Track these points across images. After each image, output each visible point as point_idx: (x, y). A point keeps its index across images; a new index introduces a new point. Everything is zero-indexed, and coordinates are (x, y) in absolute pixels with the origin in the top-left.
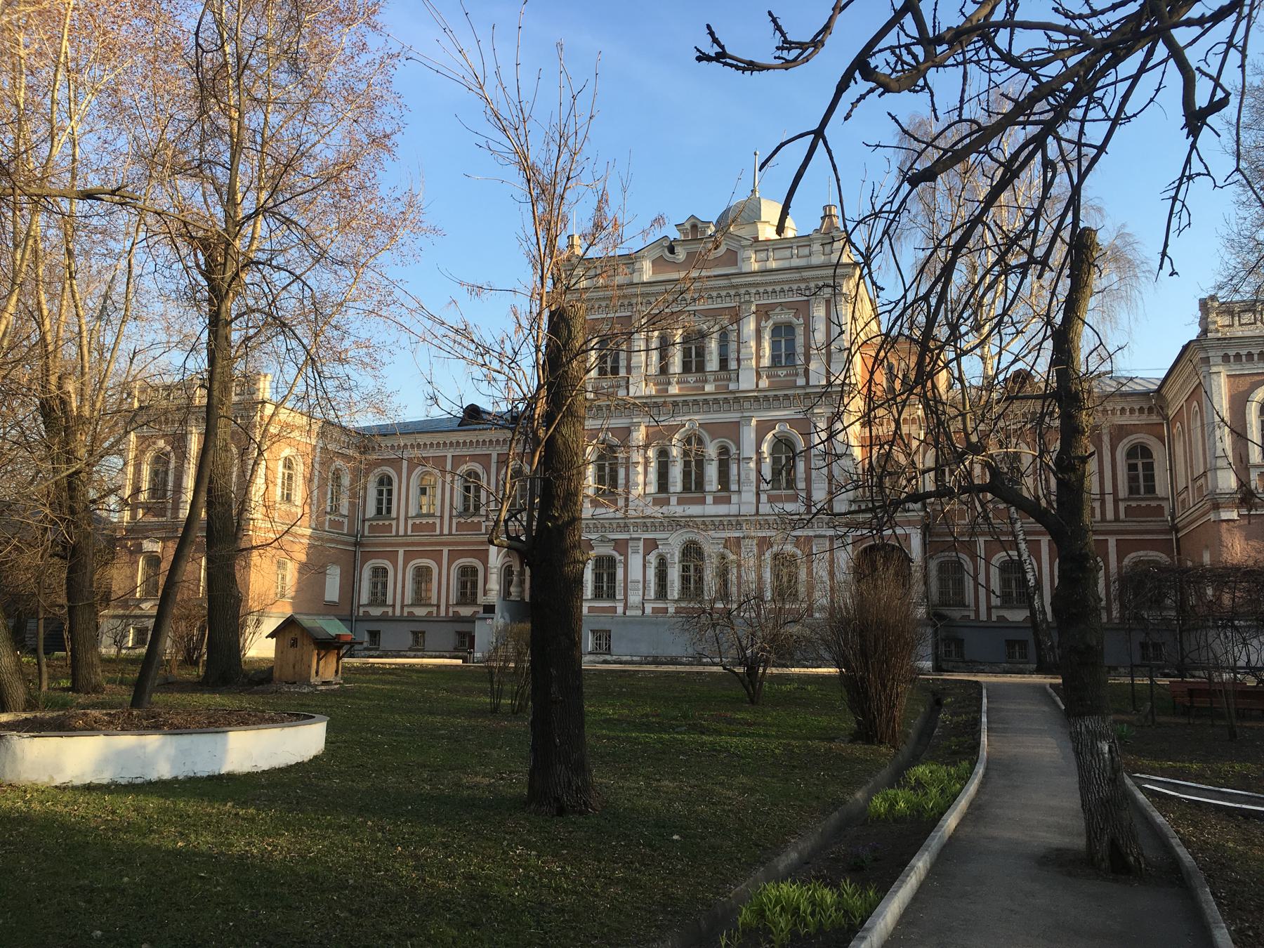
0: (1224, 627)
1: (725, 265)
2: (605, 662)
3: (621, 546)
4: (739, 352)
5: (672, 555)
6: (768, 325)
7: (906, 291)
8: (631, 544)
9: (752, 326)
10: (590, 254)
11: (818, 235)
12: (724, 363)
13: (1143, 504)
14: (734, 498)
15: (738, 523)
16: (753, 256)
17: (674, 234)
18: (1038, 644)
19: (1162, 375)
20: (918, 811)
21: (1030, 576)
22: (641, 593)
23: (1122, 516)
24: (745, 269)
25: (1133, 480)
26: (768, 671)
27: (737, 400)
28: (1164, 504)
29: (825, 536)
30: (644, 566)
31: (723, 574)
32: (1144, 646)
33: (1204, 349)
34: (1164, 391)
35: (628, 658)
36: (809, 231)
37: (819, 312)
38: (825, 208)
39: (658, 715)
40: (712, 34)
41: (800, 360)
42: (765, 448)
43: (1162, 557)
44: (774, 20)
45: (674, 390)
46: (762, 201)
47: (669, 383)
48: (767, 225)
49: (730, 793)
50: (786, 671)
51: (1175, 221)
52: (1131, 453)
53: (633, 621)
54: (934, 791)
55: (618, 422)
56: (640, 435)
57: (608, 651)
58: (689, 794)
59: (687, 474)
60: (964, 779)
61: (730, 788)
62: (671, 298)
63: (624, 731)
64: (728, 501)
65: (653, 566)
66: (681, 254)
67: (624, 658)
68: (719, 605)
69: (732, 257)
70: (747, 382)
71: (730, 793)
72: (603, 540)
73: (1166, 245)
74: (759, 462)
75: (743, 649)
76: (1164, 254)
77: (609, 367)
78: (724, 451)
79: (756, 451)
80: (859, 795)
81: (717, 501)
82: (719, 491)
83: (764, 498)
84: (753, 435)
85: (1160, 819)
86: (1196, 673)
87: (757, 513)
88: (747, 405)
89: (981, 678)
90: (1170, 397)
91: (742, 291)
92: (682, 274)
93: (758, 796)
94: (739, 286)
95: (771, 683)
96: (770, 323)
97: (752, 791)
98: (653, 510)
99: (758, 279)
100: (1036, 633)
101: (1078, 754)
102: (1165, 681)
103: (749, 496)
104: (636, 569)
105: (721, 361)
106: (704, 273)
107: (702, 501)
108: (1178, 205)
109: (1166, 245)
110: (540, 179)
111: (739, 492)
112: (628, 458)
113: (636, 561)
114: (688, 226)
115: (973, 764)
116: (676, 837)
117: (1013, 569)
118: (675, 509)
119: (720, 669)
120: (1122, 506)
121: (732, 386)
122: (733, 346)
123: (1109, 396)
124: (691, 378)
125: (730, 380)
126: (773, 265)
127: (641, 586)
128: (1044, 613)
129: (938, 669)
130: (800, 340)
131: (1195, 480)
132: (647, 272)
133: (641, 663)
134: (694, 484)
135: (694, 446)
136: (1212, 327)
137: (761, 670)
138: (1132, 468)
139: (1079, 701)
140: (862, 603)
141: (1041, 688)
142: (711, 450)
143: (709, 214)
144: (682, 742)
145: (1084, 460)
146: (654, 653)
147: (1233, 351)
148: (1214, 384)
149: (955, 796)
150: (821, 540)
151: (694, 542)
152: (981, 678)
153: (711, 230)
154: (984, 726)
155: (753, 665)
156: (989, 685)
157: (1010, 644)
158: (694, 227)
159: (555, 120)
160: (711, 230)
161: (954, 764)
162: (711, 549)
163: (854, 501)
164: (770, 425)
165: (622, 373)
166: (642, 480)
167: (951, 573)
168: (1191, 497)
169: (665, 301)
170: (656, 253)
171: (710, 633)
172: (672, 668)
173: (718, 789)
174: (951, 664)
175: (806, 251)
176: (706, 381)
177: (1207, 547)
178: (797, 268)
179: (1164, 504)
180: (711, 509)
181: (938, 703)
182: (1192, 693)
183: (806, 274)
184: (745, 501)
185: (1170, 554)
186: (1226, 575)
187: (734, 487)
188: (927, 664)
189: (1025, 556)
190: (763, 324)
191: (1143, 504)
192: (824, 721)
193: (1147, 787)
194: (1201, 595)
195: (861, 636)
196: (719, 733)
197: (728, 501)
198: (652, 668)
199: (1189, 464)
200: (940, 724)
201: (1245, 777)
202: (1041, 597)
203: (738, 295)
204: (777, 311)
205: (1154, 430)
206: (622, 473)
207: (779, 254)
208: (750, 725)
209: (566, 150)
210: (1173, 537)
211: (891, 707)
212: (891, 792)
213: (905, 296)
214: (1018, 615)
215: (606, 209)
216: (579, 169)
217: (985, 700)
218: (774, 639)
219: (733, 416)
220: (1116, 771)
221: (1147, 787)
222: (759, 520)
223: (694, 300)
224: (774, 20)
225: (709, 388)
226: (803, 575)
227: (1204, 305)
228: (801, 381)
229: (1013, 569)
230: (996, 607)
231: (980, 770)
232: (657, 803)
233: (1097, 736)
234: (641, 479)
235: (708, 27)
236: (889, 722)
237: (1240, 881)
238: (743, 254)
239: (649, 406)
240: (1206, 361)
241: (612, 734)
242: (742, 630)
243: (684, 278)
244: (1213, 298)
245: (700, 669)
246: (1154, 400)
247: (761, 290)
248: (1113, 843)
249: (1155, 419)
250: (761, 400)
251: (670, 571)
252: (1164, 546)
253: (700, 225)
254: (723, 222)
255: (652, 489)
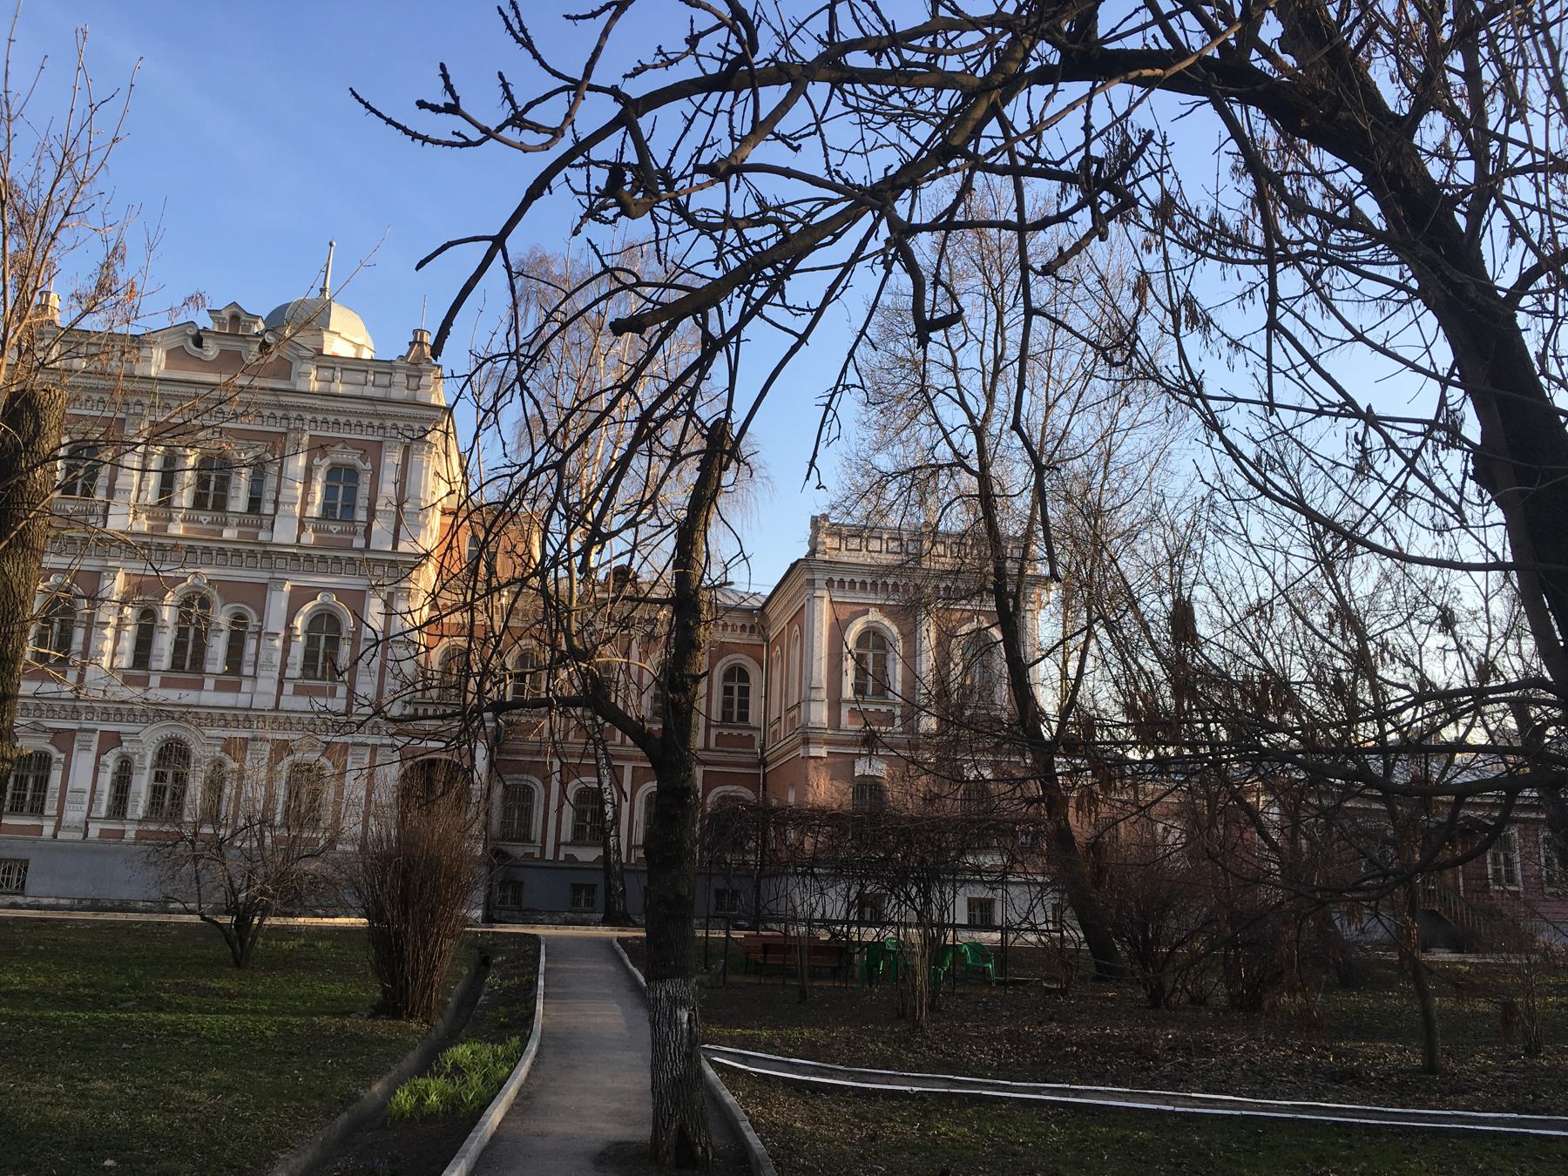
0: (804, 874)
1: (275, 376)
2: (14, 906)
3: (64, 739)
4: (278, 493)
5: (143, 757)
6: (322, 466)
7: (534, 454)
8: (79, 736)
9: (301, 460)
10: (85, 324)
11: (403, 364)
12: (255, 503)
13: (735, 733)
14: (246, 685)
15: (247, 719)
16: (314, 373)
17: (204, 321)
18: (609, 888)
19: (767, 592)
20: (453, 1105)
21: (608, 808)
22: (85, 807)
23: (712, 744)
24: (301, 386)
25: (727, 704)
26: (267, 922)
27: (269, 555)
28: (755, 734)
29: (366, 745)
30: (96, 770)
31: (215, 786)
32: (720, 894)
33: (811, 570)
34: (767, 610)
35: (52, 901)
36: (392, 356)
37: (392, 459)
38: (415, 332)
39: (92, 985)
40: (445, 77)
41: (361, 515)
42: (299, 622)
43: (747, 793)
44: (505, 86)
45: (177, 529)
46: (334, 305)
47: (170, 519)
48: (336, 338)
49: (196, 1095)
50: (291, 921)
51: (825, 429)
52: (729, 675)
53: (68, 848)
54: (475, 1079)
55: (90, 564)
56: (117, 585)
57: (21, 889)
58: (134, 1099)
59: (179, 646)
60: (513, 1060)
61: (197, 1086)
62: (202, 407)
63: (36, 1008)
64: (237, 688)
65: (110, 771)
66: (211, 350)
67: (45, 901)
68: (207, 830)
69: (284, 369)
70: (284, 533)
71: (196, 1095)
72: (36, 729)
73: (815, 455)
74: (288, 640)
75: (235, 893)
76: (812, 464)
77: (80, 483)
78: (239, 619)
79: (284, 620)
80: (377, 1087)
81: (220, 687)
82: (225, 673)
83: (288, 688)
84: (284, 604)
85: (730, 1099)
86: (769, 925)
87: (276, 708)
88: (280, 563)
89: (540, 931)
90: (773, 617)
91: (294, 414)
92: (225, 378)
93: (236, 1096)
94: (293, 407)
95: (267, 938)
96: (327, 462)
97: (229, 1090)
98: (128, 693)
99: (317, 403)
100: (607, 878)
101: (654, 1024)
102: (738, 935)
103: (267, 684)
104: (82, 776)
105: (252, 501)
106: (257, 383)
107: (199, 686)
108: (831, 413)
109: (815, 455)
110: (20, 204)
111: (255, 677)
112: (91, 616)
113: (83, 763)
114: (226, 315)
115: (525, 1041)
116: (109, 1163)
117: (590, 800)
118: (158, 694)
119: (196, 919)
120: (713, 732)
121: (263, 536)
122: (271, 483)
123: (728, 609)
124: (205, 517)
125: (261, 527)
126: (340, 389)
127: (87, 797)
128: (619, 852)
129: (489, 919)
130: (364, 490)
131: (788, 711)
132: (156, 363)
133: (71, 909)
134: (189, 657)
135: (196, 610)
136: (820, 548)
137: (256, 921)
138: (728, 691)
139: (660, 958)
140: (407, 839)
141: (608, 943)
142: (222, 617)
143: (259, 306)
144: (129, 1022)
145: (696, 679)
146: (94, 894)
147: (839, 578)
148: (817, 609)
149: (501, 1084)
150: (359, 750)
151: (179, 741)
152: (540, 931)
153: (259, 327)
154: (540, 991)
155: (243, 915)
156: (548, 938)
157: (576, 888)
158: (235, 318)
159: (59, 128)
160: (259, 327)
161: (502, 1041)
162: (204, 748)
163: (409, 703)
164: (311, 593)
165: (100, 495)
166: (111, 647)
167: (519, 799)
168: (782, 729)
169: (192, 408)
170: (175, 342)
171: (188, 868)
172: (121, 917)
173: (177, 1089)
174: (504, 913)
175: (385, 380)
176: (226, 524)
177: (793, 785)
178: (371, 399)
179: (755, 734)
180: (209, 696)
181: (485, 963)
182: (767, 948)
183: (381, 408)
184: (261, 690)
185: (756, 792)
186: (810, 818)
187: (248, 670)
188: (478, 913)
189: (606, 784)
190: (316, 461)
191: (735, 733)
192: (337, 989)
193: (719, 1059)
194: (782, 837)
195: (404, 877)
196: (185, 1009)
197: (237, 688)
198: (89, 916)
199: (785, 694)
200: (486, 989)
201: (814, 1045)
202: (618, 836)
203: (348, 424)
204: (338, 447)
205: (753, 651)
206: (79, 635)
207: (348, 376)
208: (231, 997)
209: (69, 173)
210: (760, 772)
211: (430, 970)
212: (421, 1082)
213: (531, 461)
214: (588, 855)
215: (118, 268)
216: (86, 204)
217: (543, 959)
218: (281, 878)
219: (260, 576)
220: (694, 1042)
221: (719, 1059)
222: (278, 717)
223: (236, 416)
224: (505, 86)
225: (228, 534)
226: (329, 794)
227: (815, 523)
228: (359, 543)
229: (590, 800)
230: (566, 844)
231: (533, 1047)
232: (83, 1114)
233: (676, 1002)
234: (108, 646)
235: (442, 67)
236: (425, 988)
237: (808, 1168)
238: (299, 367)
239: (129, 546)
240: (811, 582)
241: (16, 1013)
242: (234, 863)
243: (226, 384)
244: (825, 517)
245: (163, 918)
246: (757, 617)
247: (320, 418)
248: (682, 1131)
249: (756, 639)
250: (300, 559)
251: (135, 779)
252: (749, 781)
253: (243, 318)
254: (277, 319)
255: (125, 661)
